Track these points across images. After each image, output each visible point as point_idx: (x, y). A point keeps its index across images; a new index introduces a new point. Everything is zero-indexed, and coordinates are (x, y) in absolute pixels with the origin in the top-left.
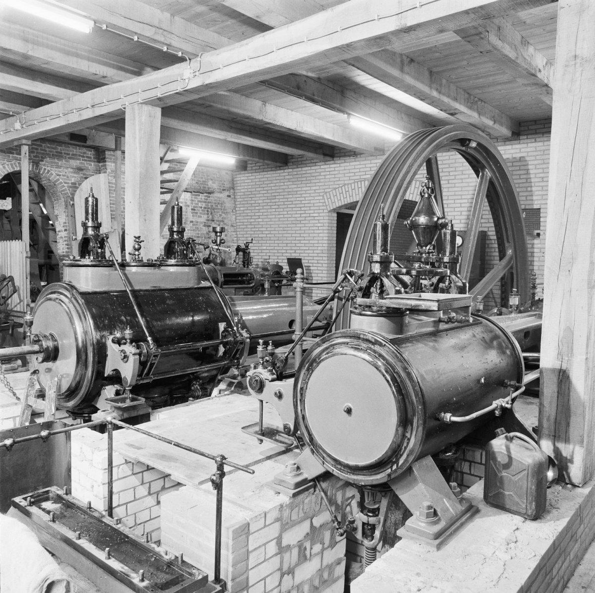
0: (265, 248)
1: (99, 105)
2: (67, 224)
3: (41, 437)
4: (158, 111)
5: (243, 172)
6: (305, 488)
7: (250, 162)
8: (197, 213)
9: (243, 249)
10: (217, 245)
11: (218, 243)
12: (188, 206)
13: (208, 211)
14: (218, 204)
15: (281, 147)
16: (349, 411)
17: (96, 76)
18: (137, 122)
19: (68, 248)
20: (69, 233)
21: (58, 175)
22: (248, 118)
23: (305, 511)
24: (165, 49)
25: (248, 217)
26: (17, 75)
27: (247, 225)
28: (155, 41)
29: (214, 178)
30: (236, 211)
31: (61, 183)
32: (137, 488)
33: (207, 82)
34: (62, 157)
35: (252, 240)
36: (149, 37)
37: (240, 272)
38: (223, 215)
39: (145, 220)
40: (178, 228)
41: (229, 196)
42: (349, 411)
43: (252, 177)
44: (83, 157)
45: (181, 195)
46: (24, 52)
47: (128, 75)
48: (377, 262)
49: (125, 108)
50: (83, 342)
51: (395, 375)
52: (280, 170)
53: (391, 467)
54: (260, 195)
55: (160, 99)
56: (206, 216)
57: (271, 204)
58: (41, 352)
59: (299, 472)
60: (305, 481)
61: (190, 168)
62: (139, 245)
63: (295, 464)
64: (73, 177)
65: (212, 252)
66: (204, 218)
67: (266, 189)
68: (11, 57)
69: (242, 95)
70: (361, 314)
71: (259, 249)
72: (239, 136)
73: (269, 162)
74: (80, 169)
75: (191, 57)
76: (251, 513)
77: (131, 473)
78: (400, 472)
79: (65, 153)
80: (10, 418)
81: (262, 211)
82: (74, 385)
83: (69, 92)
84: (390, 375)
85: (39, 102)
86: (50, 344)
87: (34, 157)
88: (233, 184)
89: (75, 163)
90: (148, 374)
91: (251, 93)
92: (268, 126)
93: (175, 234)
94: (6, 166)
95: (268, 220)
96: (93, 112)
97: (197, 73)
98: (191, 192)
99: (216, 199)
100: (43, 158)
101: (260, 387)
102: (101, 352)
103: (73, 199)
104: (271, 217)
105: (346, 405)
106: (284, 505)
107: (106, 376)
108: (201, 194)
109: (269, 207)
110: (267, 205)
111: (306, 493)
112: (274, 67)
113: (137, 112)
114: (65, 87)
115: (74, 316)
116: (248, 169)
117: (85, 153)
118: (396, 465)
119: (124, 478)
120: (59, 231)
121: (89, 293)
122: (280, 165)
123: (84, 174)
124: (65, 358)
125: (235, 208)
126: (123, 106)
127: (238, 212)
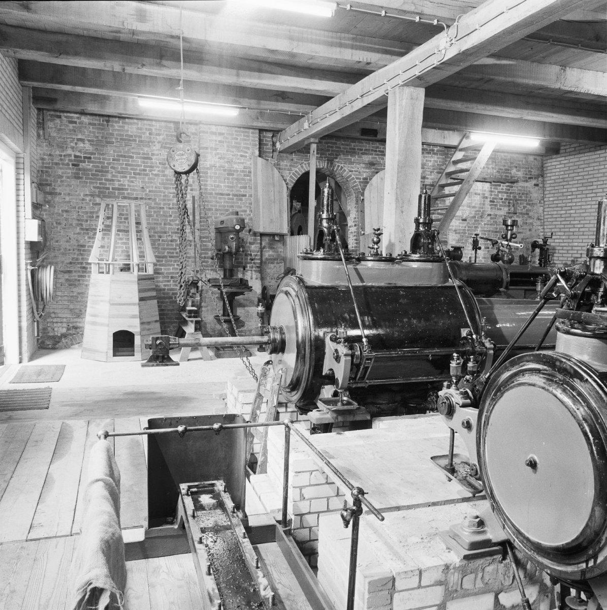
0: (576, 244)
1: (367, 94)
2: (357, 220)
3: (213, 429)
4: (421, 92)
5: (555, 156)
6: (481, 553)
7: (564, 144)
8: (496, 205)
9: (541, 244)
10: (507, 241)
11: (509, 238)
12: (487, 198)
13: (509, 203)
14: (523, 194)
15: (596, 120)
16: (533, 465)
17: (359, 64)
18: (397, 107)
19: (356, 243)
20: (358, 229)
21: (351, 171)
22: (541, 88)
23: (486, 581)
24: (417, 19)
25: (558, 209)
26: (298, 76)
27: (556, 218)
28: (405, 12)
29: (519, 165)
30: (544, 202)
31: (353, 179)
32: (331, 499)
33: (463, 49)
34: (355, 153)
35: (552, 234)
36: (396, 9)
37: (531, 272)
38: (528, 206)
39: (402, 212)
40: (425, 219)
41: (536, 185)
42: (533, 465)
43: (566, 162)
44: (376, 151)
45: (471, 185)
46: (288, 50)
47: (394, 57)
48: (598, 258)
49: (387, 94)
50: (302, 337)
51: (597, 426)
52: (601, 150)
53: (587, 562)
54: (574, 182)
55: (419, 78)
56: (506, 209)
57: (587, 192)
58: (269, 344)
59: (480, 529)
60: (487, 543)
61: (483, 157)
62: (378, 238)
63: (477, 517)
64: (365, 172)
65: (501, 248)
66: (504, 211)
67: (582, 174)
68: (280, 58)
69: (533, 62)
70: (568, 333)
71: (569, 246)
72: (536, 112)
73: (586, 142)
74: (372, 164)
75: (450, 23)
76: (402, 566)
77: (324, 482)
78: (597, 572)
79: (358, 149)
80: (250, 404)
81: (575, 200)
82: (295, 379)
83: (344, 85)
84: (589, 425)
85: (321, 100)
86: (278, 337)
87: (329, 154)
88: (542, 170)
89: (367, 158)
90: (363, 378)
91: (544, 58)
92: (569, 95)
93: (421, 225)
94: (304, 166)
95: (581, 211)
96: (363, 101)
97: (453, 42)
98: (490, 182)
99: (519, 188)
100: (338, 155)
101: (450, 412)
102: (318, 346)
103: (363, 194)
104: (586, 207)
105: (531, 455)
106: (451, 567)
107: (324, 374)
108: (502, 184)
109: (584, 196)
110: (582, 194)
111: (488, 558)
112: (538, 13)
113: (397, 96)
114: (342, 82)
115: (297, 311)
116: (561, 151)
117: (377, 147)
118: (593, 560)
119: (316, 485)
120: (350, 227)
121: (315, 288)
122: (600, 143)
123: (375, 169)
124: (289, 352)
125: (543, 198)
126: (387, 92)
127: (546, 203)
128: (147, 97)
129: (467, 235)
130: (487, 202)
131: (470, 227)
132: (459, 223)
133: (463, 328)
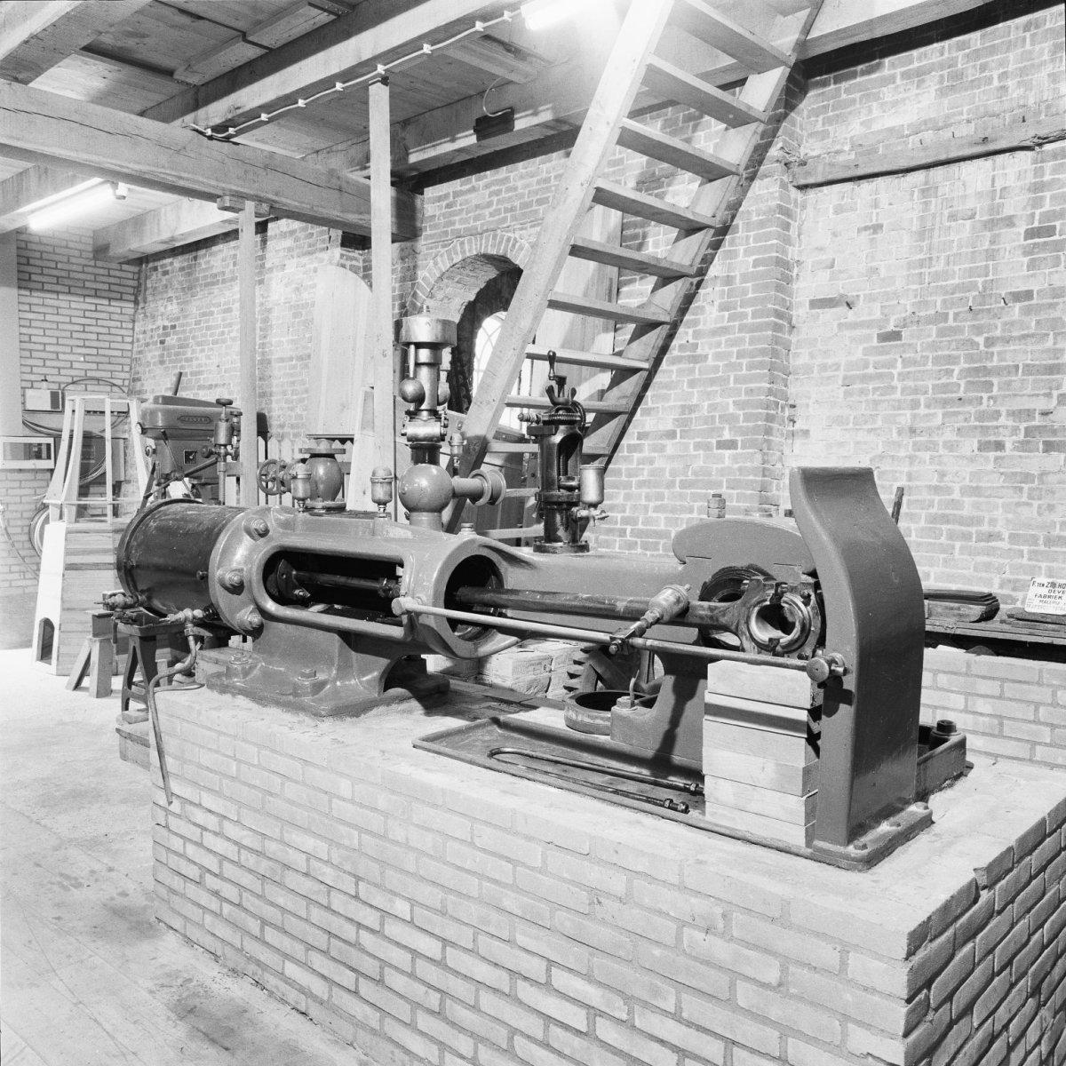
12: (1010, 222)
128: (41, 208)
129: (898, 395)
130: (1013, 238)
131: (915, 363)
132: (867, 352)
133: (676, 680)
